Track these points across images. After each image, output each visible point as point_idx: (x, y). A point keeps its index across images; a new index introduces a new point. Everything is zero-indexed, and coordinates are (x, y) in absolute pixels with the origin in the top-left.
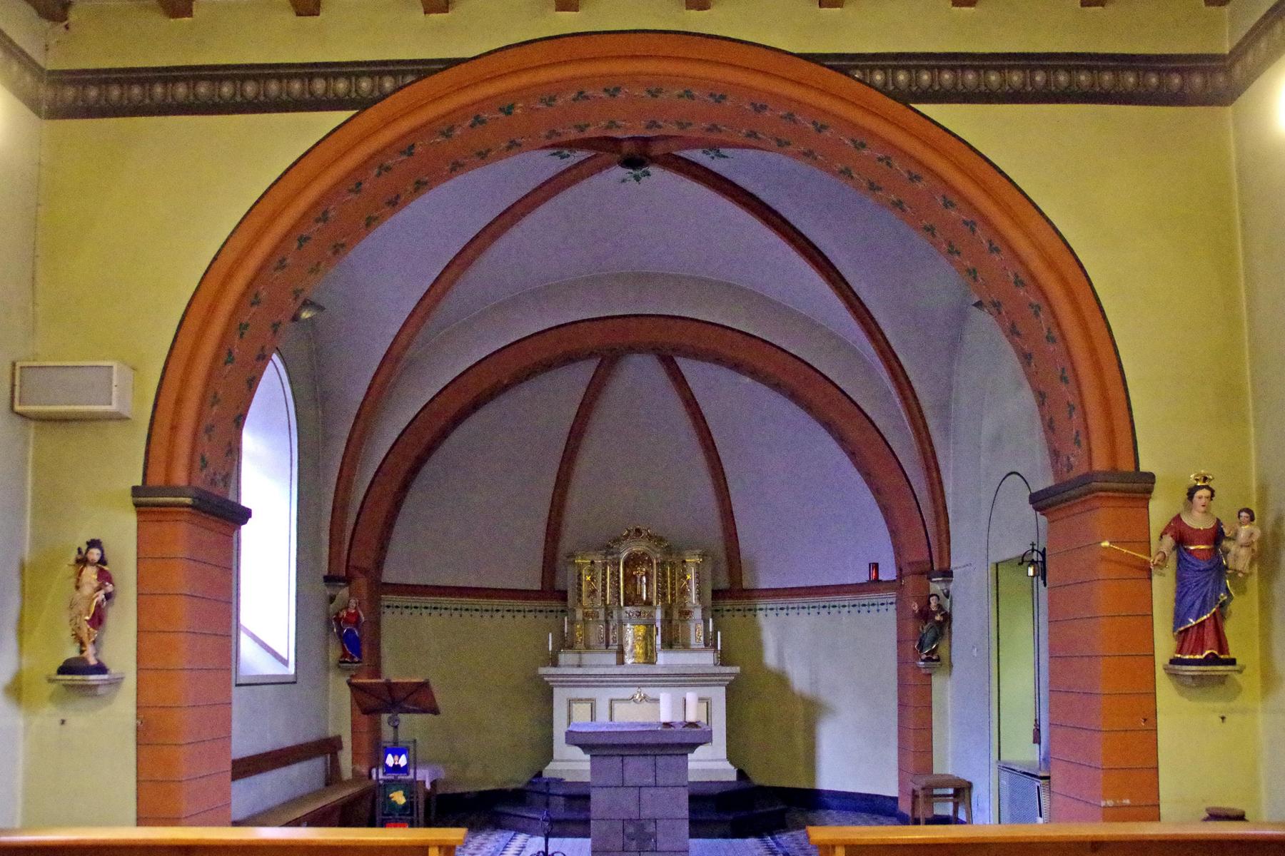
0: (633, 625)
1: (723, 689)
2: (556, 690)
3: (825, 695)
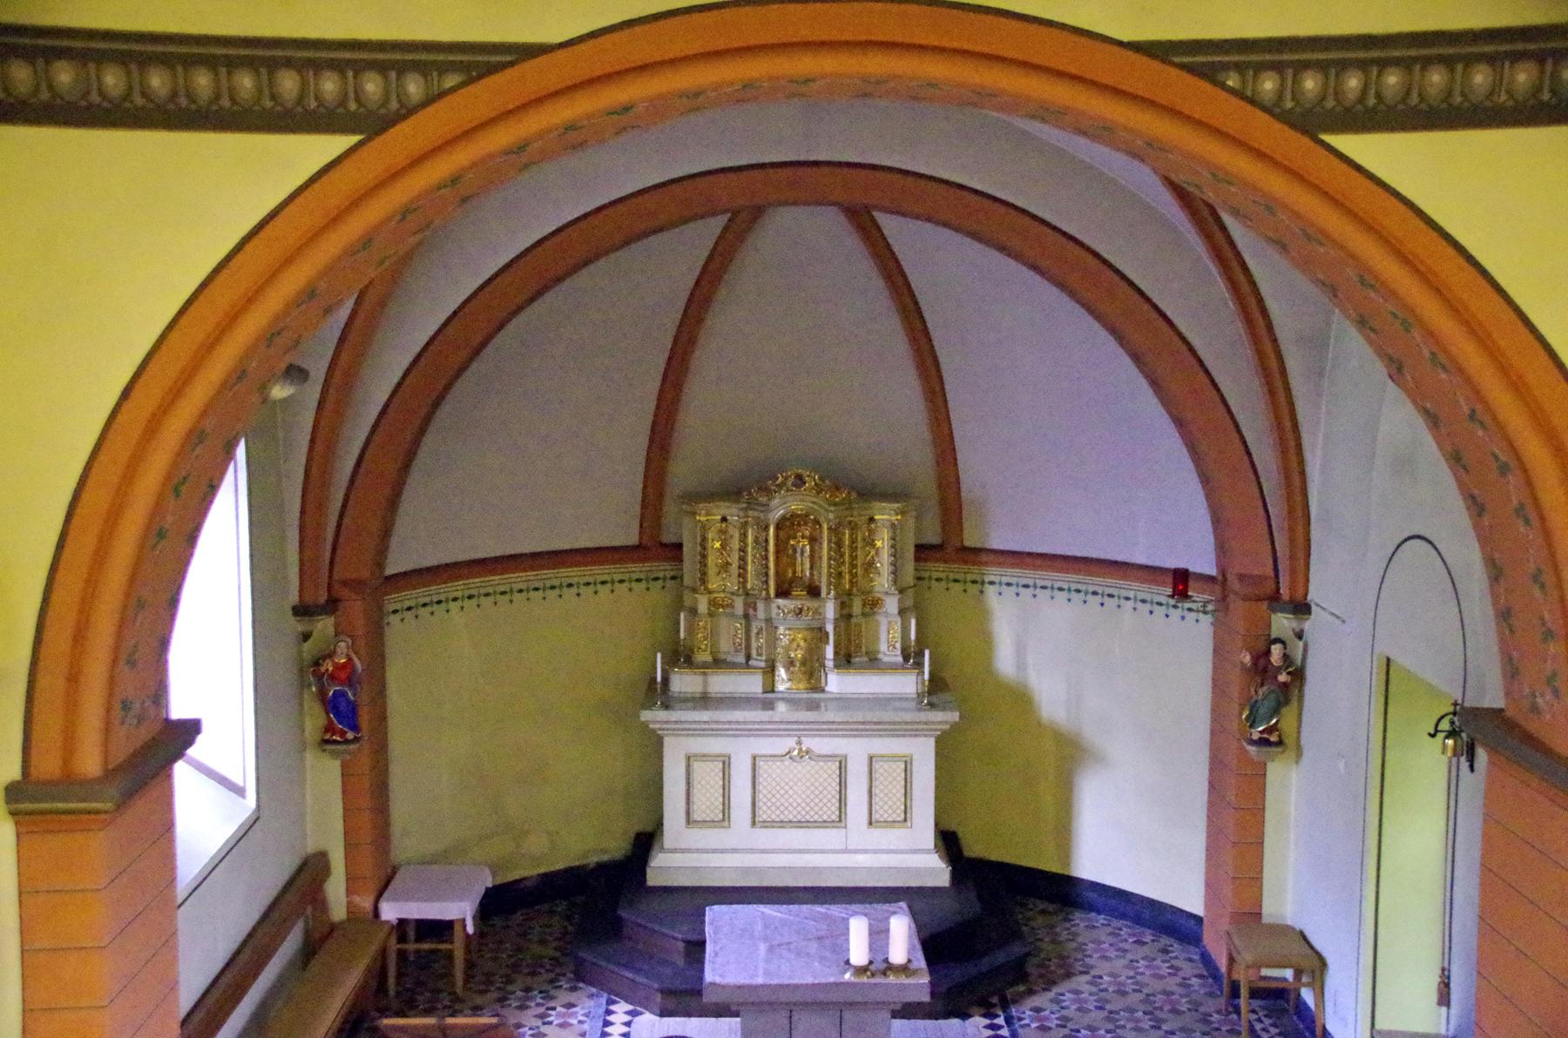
0: (789, 629)
1: (932, 742)
2: (667, 741)
3: (1092, 734)
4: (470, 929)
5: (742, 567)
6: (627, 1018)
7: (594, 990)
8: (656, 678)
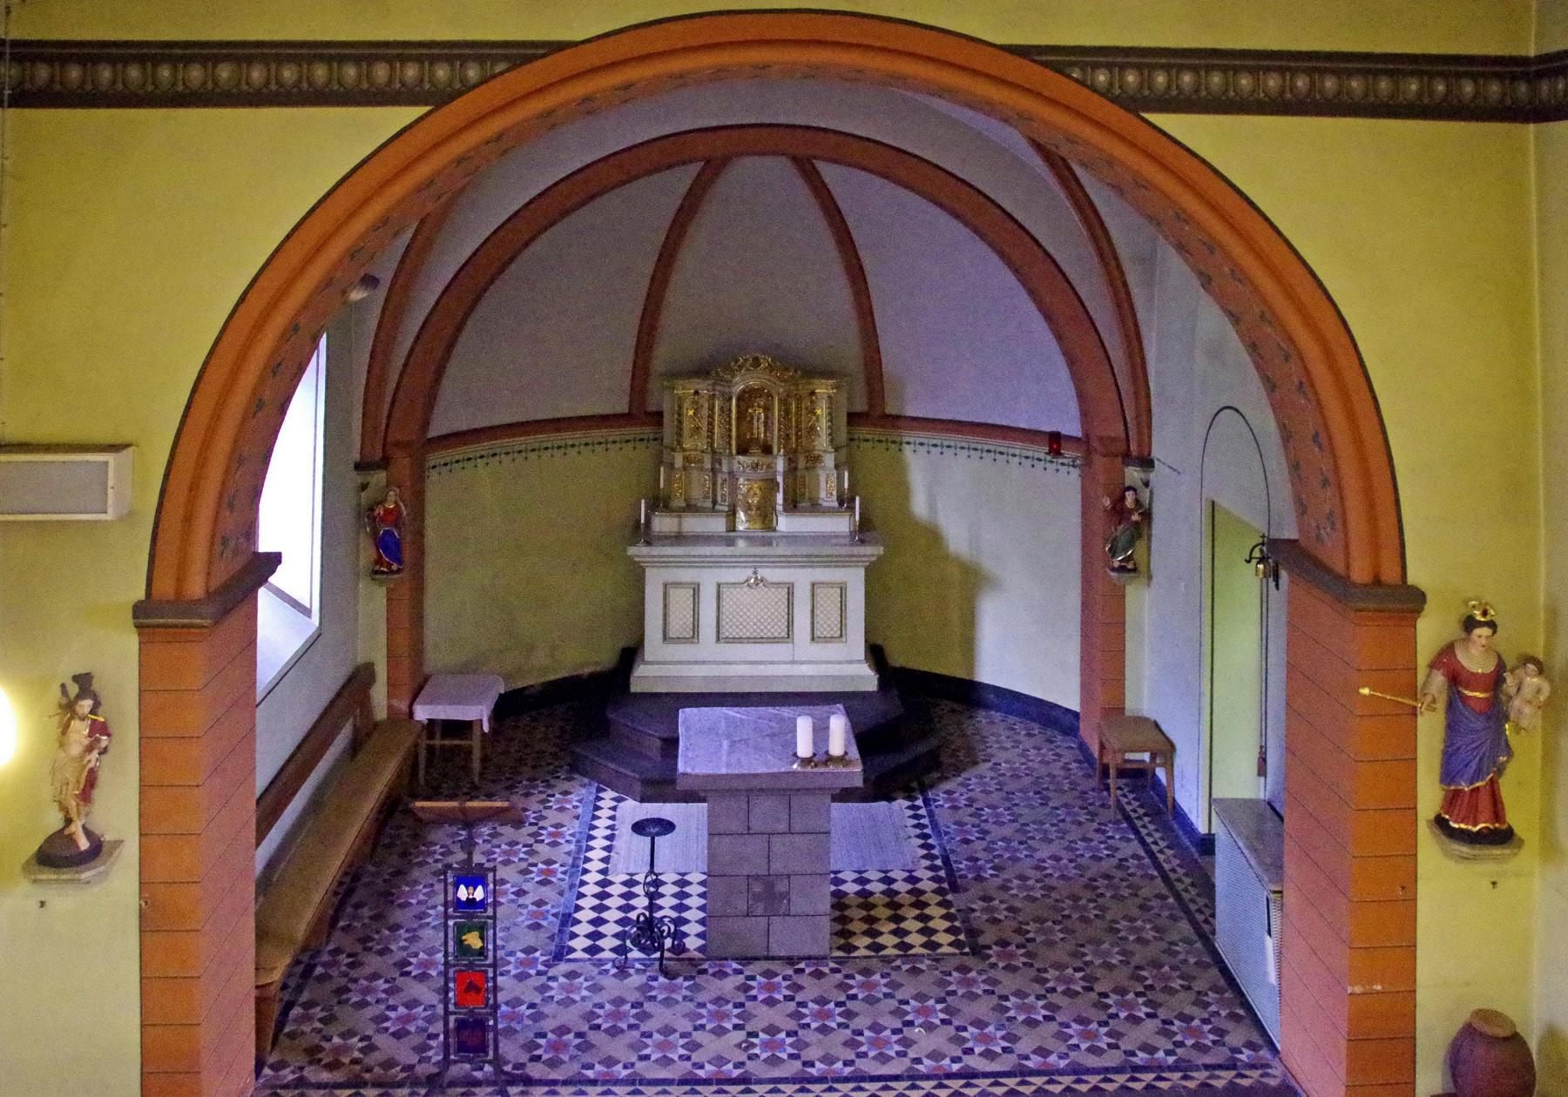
0: (748, 480)
1: (862, 572)
3: (988, 565)
4: (486, 728)
5: (711, 431)
6: (614, 804)
7: (586, 780)
8: (640, 521)
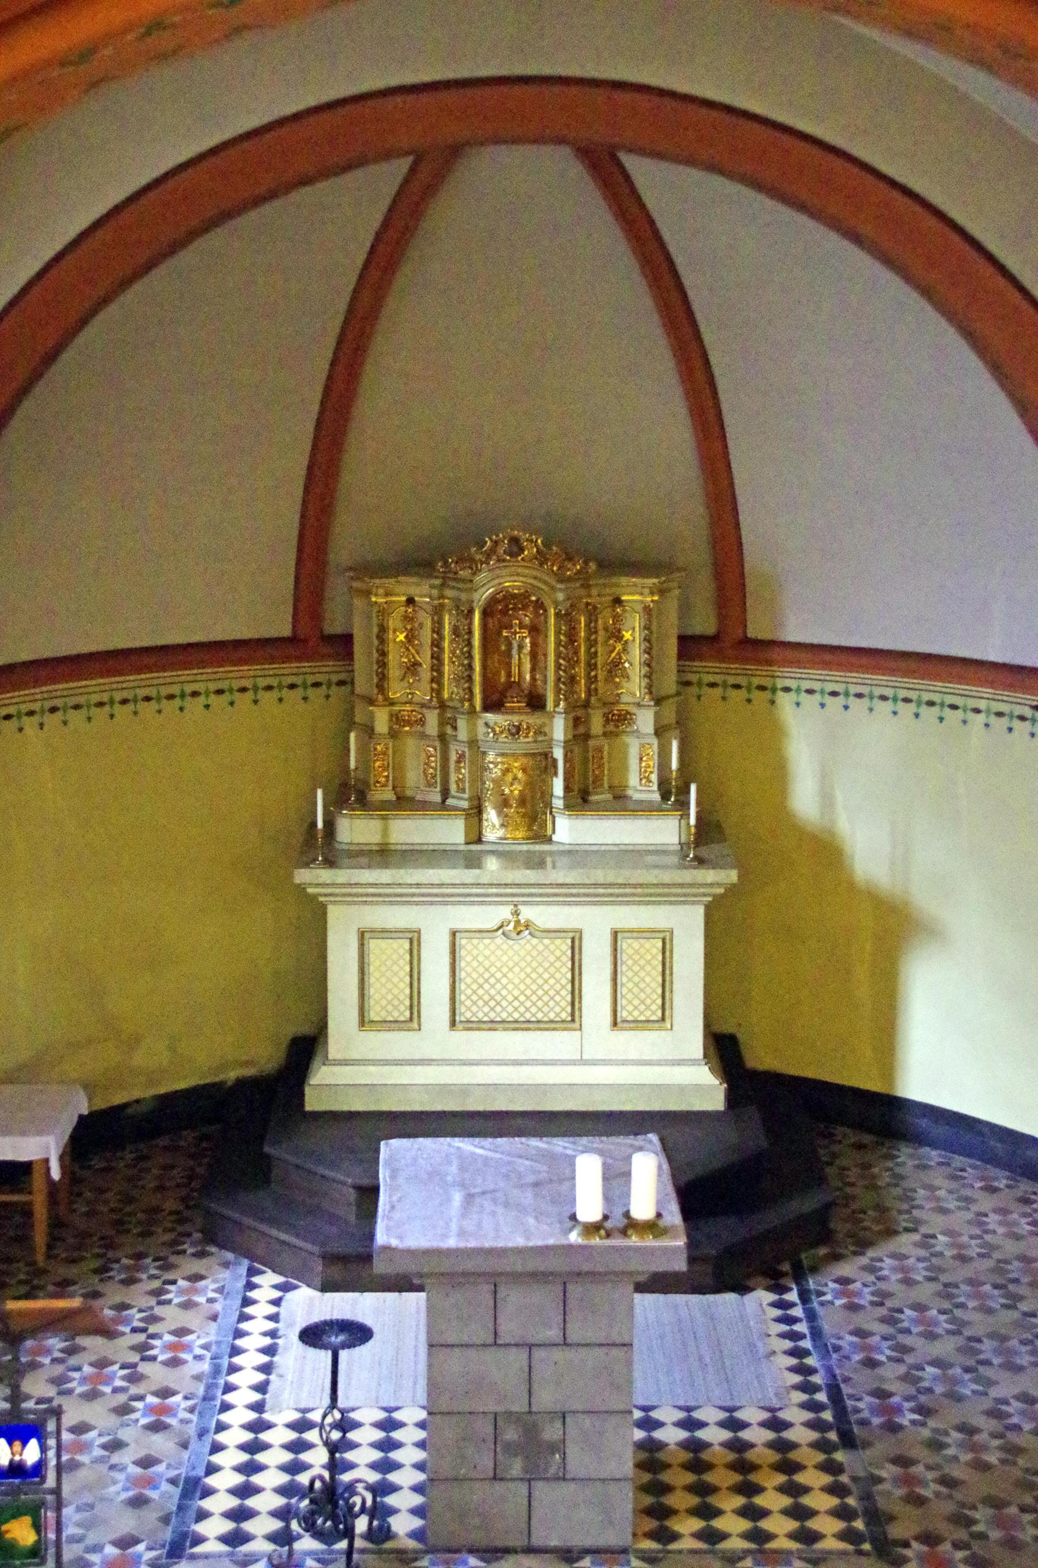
1: (700, 910)
